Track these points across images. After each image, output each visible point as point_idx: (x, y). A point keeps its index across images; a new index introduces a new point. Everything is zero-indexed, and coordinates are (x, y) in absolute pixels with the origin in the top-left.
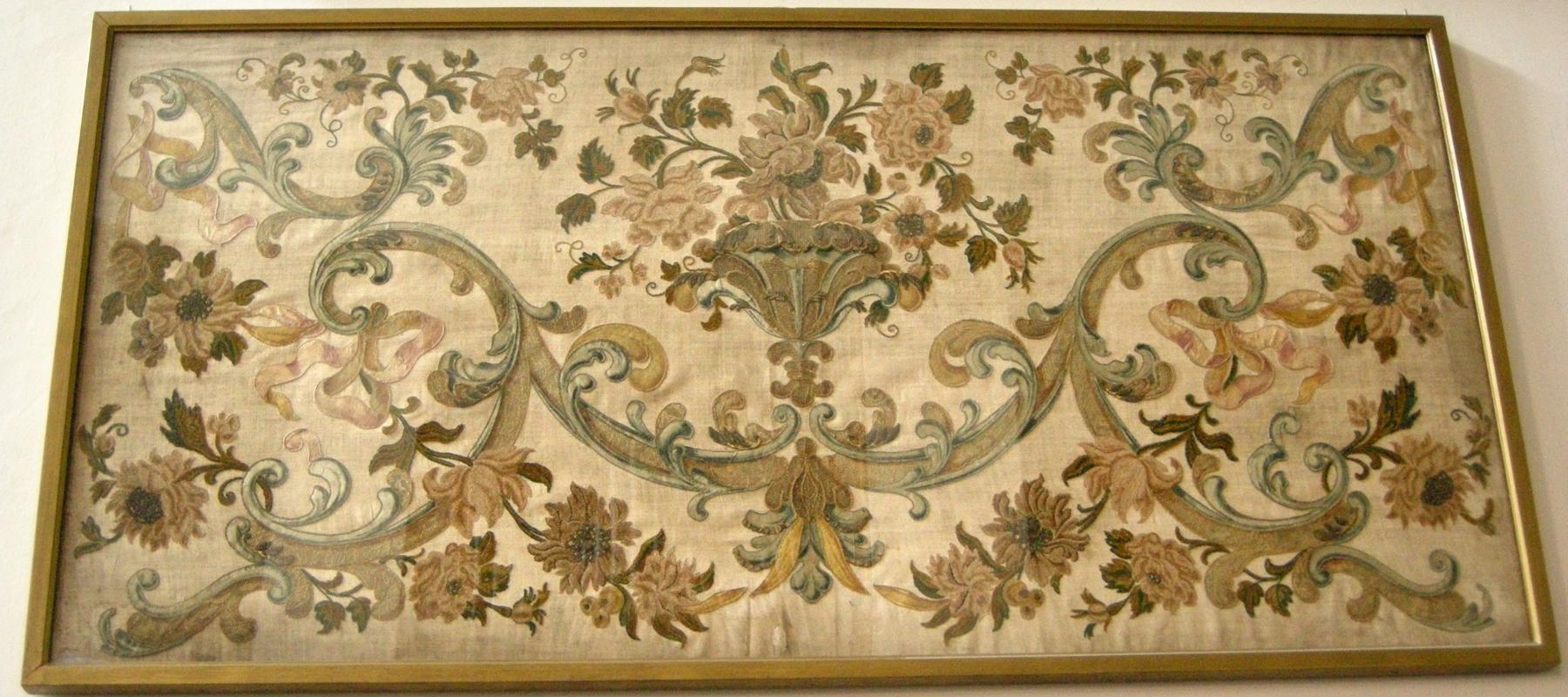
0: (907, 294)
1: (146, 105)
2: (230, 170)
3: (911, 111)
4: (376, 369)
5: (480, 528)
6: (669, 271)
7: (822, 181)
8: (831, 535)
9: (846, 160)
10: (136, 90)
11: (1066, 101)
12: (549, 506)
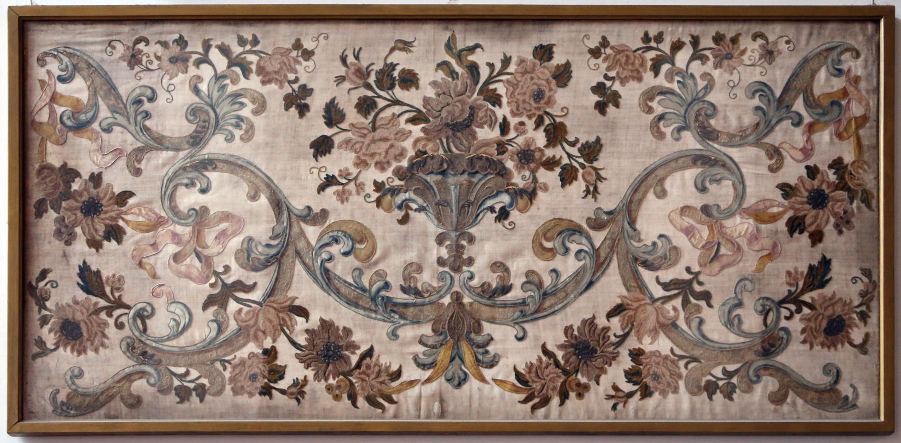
0: (521, 202)
1: (48, 72)
2: (107, 118)
3: (532, 78)
4: (204, 248)
5: (268, 343)
6: (378, 186)
7: (474, 127)
8: (469, 350)
9: (489, 113)
10: (42, 62)
11: (632, 71)
12: (307, 331)
